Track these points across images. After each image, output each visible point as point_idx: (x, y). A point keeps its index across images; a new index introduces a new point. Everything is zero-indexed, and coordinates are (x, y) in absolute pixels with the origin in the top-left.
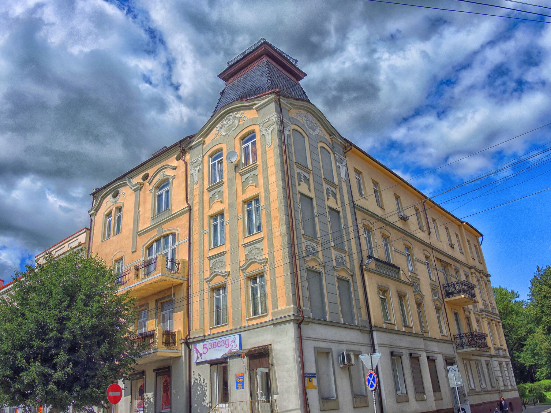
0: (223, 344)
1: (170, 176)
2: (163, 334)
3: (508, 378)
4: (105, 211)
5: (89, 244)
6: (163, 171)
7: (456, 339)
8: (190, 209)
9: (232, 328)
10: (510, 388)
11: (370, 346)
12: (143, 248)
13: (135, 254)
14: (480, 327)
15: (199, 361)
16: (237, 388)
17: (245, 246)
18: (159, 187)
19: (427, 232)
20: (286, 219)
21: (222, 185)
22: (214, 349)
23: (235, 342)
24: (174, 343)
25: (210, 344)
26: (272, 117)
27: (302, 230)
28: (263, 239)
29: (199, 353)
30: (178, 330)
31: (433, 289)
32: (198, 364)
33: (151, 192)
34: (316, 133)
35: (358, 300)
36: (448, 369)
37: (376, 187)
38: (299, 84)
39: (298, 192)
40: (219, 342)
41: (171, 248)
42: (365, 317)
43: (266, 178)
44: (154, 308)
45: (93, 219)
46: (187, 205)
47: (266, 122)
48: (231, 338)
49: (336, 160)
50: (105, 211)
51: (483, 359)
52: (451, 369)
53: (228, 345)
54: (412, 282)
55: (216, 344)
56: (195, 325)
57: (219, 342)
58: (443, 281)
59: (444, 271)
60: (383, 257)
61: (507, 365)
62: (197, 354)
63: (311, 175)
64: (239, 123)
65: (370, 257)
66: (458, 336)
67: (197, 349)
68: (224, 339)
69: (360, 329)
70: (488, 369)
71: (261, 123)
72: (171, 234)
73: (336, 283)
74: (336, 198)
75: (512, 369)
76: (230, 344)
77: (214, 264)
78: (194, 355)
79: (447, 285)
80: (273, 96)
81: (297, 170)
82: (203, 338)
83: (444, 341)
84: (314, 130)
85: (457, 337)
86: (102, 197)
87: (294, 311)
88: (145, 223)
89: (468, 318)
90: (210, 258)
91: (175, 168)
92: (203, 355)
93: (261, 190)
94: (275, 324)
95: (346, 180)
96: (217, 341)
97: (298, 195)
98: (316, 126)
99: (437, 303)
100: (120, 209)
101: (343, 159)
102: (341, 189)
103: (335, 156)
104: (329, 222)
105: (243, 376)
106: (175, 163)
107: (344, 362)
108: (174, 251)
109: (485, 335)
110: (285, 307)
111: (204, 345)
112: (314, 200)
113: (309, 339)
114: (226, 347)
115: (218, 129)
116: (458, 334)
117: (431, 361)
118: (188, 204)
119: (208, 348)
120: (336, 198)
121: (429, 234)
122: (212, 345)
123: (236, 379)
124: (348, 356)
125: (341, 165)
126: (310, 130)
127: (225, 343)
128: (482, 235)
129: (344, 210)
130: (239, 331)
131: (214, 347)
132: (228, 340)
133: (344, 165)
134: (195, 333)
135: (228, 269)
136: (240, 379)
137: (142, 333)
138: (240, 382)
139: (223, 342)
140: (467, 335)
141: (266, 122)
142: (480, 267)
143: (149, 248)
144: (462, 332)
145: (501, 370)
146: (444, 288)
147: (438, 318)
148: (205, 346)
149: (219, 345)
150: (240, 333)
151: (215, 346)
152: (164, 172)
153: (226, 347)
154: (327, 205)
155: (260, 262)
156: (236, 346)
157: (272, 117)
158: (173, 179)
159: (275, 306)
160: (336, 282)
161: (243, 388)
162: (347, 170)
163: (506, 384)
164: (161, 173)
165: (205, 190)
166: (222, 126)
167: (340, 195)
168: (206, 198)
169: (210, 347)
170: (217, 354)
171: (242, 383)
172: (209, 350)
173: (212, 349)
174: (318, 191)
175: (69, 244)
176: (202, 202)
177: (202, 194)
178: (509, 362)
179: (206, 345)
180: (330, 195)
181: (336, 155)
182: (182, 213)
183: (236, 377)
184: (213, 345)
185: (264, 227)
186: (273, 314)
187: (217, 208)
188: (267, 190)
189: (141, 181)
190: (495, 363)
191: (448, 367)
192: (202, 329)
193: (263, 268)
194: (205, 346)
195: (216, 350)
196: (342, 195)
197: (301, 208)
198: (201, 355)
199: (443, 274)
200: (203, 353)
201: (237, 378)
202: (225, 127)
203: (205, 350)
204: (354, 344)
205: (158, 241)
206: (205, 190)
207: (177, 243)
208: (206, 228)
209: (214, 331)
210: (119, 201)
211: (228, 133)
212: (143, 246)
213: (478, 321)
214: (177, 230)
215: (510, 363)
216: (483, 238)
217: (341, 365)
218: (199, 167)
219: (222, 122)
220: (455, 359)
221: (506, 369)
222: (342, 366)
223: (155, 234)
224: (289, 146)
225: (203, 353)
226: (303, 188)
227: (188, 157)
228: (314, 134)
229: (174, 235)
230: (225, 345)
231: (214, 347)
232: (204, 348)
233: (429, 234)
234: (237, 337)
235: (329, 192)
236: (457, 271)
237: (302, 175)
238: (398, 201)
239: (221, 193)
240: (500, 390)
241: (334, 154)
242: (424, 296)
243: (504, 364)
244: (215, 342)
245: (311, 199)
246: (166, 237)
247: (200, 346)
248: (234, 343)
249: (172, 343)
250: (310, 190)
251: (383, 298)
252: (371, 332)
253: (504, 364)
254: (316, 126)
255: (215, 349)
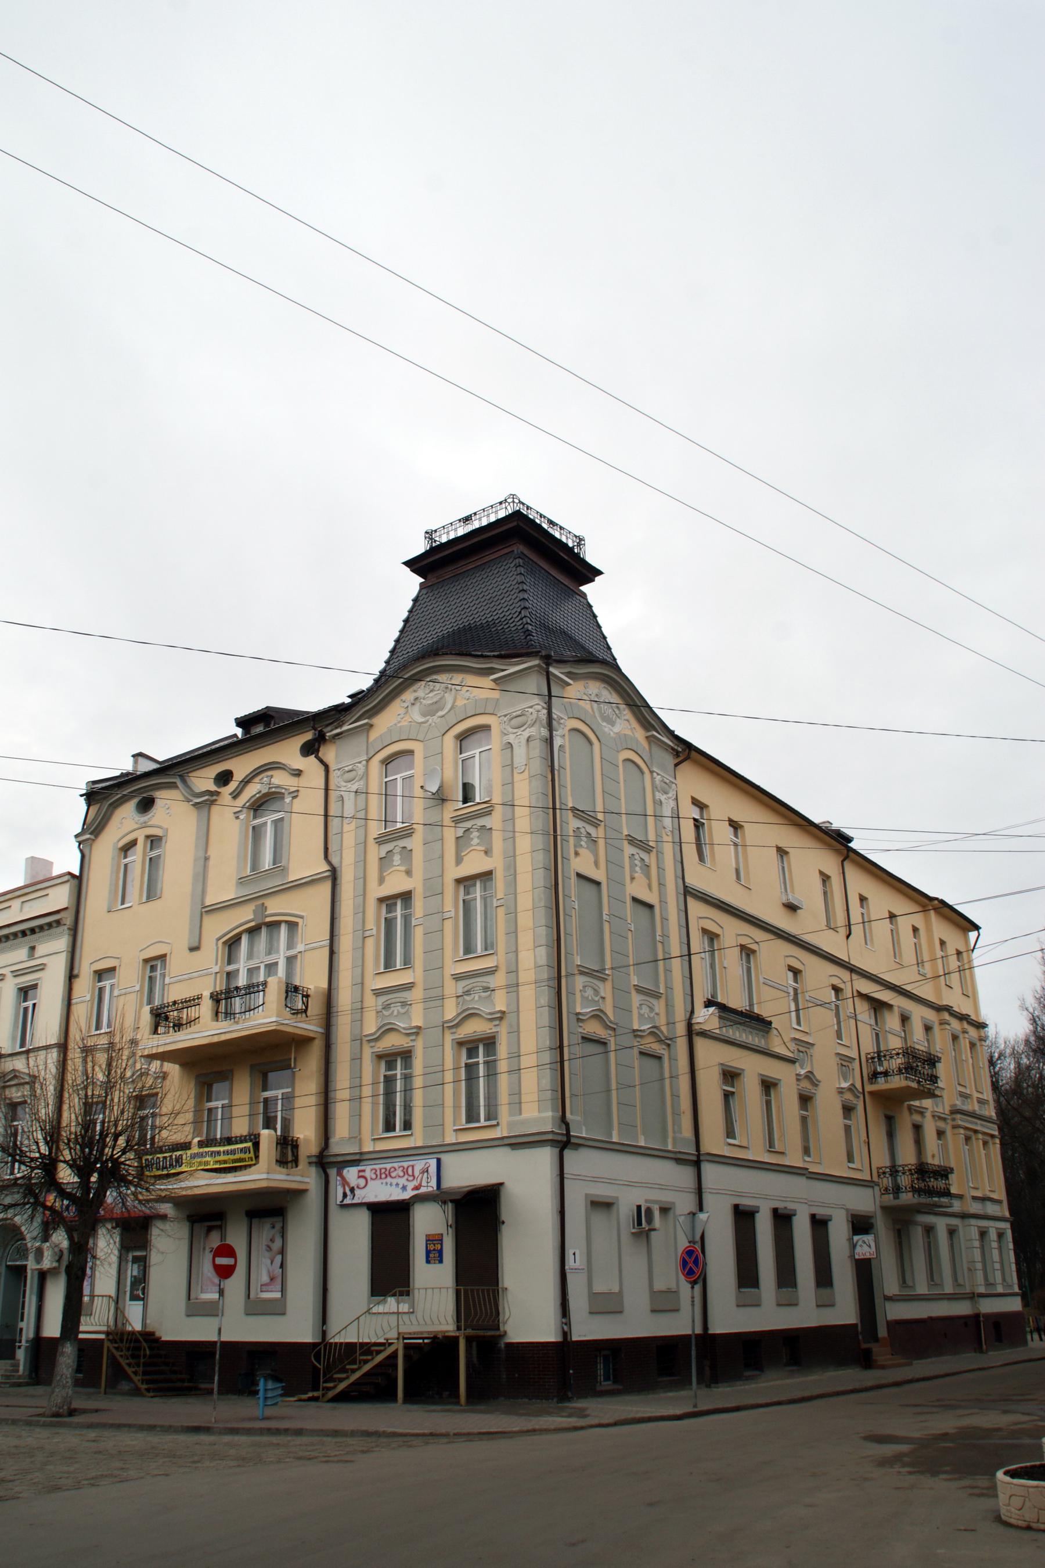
0: (401, 1174)
1: (286, 789)
2: (277, 1144)
3: (997, 1266)
4: (120, 839)
5: (77, 912)
6: (270, 773)
7: (882, 1176)
8: (334, 875)
9: (420, 1144)
10: (1000, 1289)
11: (693, 1191)
12: (217, 944)
13: (195, 953)
14: (945, 1148)
15: (348, 1201)
16: (428, 1262)
17: (458, 978)
18: (258, 806)
19: (843, 932)
20: (547, 935)
21: (410, 835)
22: (381, 1181)
23: (427, 1171)
24: (296, 1161)
25: (374, 1171)
26: (531, 707)
27: (577, 955)
28: (496, 970)
29: (348, 1185)
30: (305, 1136)
31: (842, 1065)
32: (343, 1206)
33: (237, 818)
34: (617, 729)
35: (675, 1096)
36: (855, 1242)
37: (736, 836)
38: (584, 596)
39: (572, 872)
40: (392, 1170)
41: (285, 953)
42: (687, 1132)
43: (511, 837)
44: (77, 1003)
45: (87, 852)
46: (327, 868)
47: (516, 717)
48: (419, 1165)
49: (654, 787)
50: (120, 839)
51: (941, 1224)
52: (860, 1243)
53: (413, 1175)
54: (796, 1051)
55: (387, 1173)
56: (341, 1128)
57: (392, 1170)
58: (868, 1046)
59: (873, 1022)
60: (737, 1001)
61: (1001, 1235)
62: (344, 1189)
63: (601, 829)
64: (454, 702)
65: (709, 1004)
66: (888, 1170)
67: (343, 1178)
68: (405, 1164)
69: (679, 1160)
70: (952, 1246)
71: (505, 716)
72: (286, 922)
73: (636, 1063)
74: (648, 876)
75: (1011, 1246)
76: (417, 1173)
77: (386, 1007)
78: (337, 1192)
79: (876, 1055)
80: (536, 662)
81: (574, 823)
82: (357, 1157)
83: (850, 1181)
84: (612, 723)
85: (884, 1173)
86: (111, 805)
87: (553, 1124)
88: (223, 889)
89: (917, 1128)
90: (378, 993)
91: (298, 773)
92: (357, 1192)
93: (494, 863)
94: (518, 1143)
95: (672, 832)
96: (388, 1166)
97: (573, 877)
98: (617, 712)
99: (848, 1096)
100: (154, 841)
101: (671, 782)
102: (660, 853)
103: (653, 779)
104: (630, 932)
105: (441, 1240)
106: (298, 761)
107: (640, 1223)
108: (290, 960)
109: (949, 1170)
110: (535, 1114)
111: (360, 1171)
112: (604, 887)
113: (577, 1177)
114: (407, 1180)
115: (405, 705)
116: (888, 1164)
117: (819, 1224)
118: (329, 863)
119: (369, 1179)
120: (648, 876)
121: (848, 937)
122: (378, 1173)
123: (427, 1244)
124: (649, 1211)
125: (665, 796)
126: (604, 724)
127: (405, 1171)
128: (977, 928)
129: (663, 901)
130: (438, 1151)
131: (381, 1178)
132: (413, 1166)
133: (670, 795)
134: (340, 1146)
135: (417, 1021)
136: (434, 1245)
137: (232, 1137)
138: (434, 1250)
139: (401, 1169)
140: (906, 1168)
141: (516, 717)
142: (962, 1006)
143: (232, 944)
144: (900, 1161)
145: (982, 1247)
146: (867, 1061)
147: (847, 1129)
148: (361, 1174)
149: (393, 1174)
150: (438, 1156)
151: (383, 1176)
152: (272, 776)
153: (407, 1180)
154: (630, 894)
155: (490, 1017)
156: (429, 1180)
157: (531, 707)
158: (294, 797)
159: (517, 1104)
160: (636, 1061)
161: (441, 1261)
162: (676, 808)
163: (991, 1281)
164: (264, 777)
165: (371, 841)
166: (416, 699)
167: (658, 868)
168: (374, 853)
169: (374, 1176)
170: (395, 1195)
171: (440, 1252)
172: (370, 1183)
173: (379, 1182)
174: (613, 864)
175: (23, 902)
176: (362, 861)
177: (363, 846)
178: (1005, 1229)
179: (364, 1171)
180: (638, 869)
181: (655, 774)
182: (313, 881)
183: (427, 1241)
184: (381, 1174)
185: (501, 943)
186: (510, 1125)
187: (396, 884)
188: (511, 858)
189: (213, 788)
190: (970, 1231)
191: (856, 1238)
192: (356, 1137)
193: (494, 1030)
194: (361, 1174)
195: (387, 1183)
196: (660, 868)
197: (576, 907)
198: (352, 1190)
199: (868, 1027)
200: (358, 1187)
201: (429, 1242)
202: (421, 703)
203: (362, 1182)
204: (661, 1187)
205: (253, 931)
206: (371, 841)
207: (300, 947)
208: (371, 924)
209: (381, 1146)
210: (154, 821)
211: (428, 721)
212: (218, 939)
213: (940, 1134)
214: (302, 917)
215: (1009, 1233)
216: (979, 935)
217: (634, 1228)
218: (357, 784)
219: (415, 691)
220: (873, 1221)
221: (995, 1245)
222: (634, 1231)
223: (245, 915)
224: (562, 770)
225: (358, 1187)
226: (583, 863)
227: (329, 753)
228: (612, 733)
229: (292, 926)
230: (406, 1176)
231: (381, 1178)
232: (359, 1177)
233: (848, 937)
234: (433, 1163)
235: (636, 862)
236: (905, 1019)
237: (582, 830)
238: (782, 862)
239: (407, 853)
240: (974, 1293)
241: (652, 772)
242: (819, 1082)
243: (993, 1235)
244: (386, 1169)
245: (598, 884)
246: (274, 925)
247: (351, 1174)
248: (426, 1174)
249: (291, 1161)
250: (596, 864)
251: (727, 1091)
252: (697, 1164)
253: (993, 1235)
254: (617, 712)
255: (384, 1181)
